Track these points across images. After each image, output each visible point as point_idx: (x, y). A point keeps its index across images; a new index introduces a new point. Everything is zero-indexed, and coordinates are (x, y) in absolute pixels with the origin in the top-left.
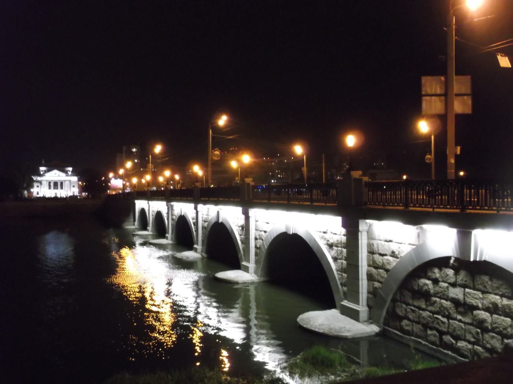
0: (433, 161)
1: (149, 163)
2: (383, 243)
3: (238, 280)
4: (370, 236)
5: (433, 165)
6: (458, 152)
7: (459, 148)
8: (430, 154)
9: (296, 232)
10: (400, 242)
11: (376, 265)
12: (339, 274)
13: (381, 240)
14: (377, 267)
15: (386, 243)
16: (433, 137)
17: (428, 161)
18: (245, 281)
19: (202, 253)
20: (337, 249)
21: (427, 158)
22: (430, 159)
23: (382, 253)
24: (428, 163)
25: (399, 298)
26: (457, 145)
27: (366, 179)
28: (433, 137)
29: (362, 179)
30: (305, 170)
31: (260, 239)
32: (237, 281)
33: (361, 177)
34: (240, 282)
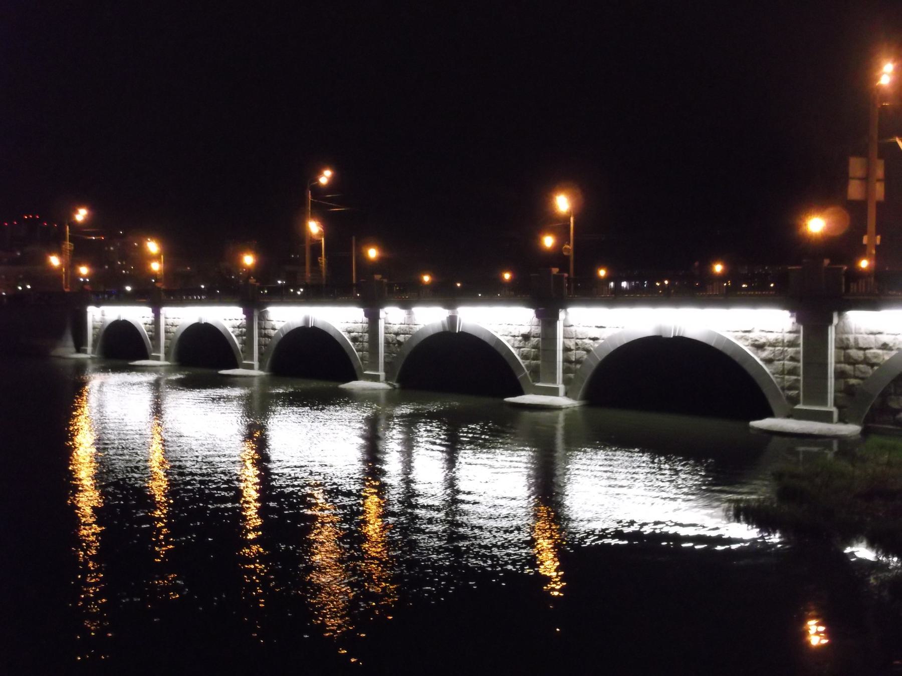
0: (571, 253)
1: (65, 239)
2: (866, 336)
3: (561, 405)
4: (840, 330)
5: (572, 258)
6: (878, 242)
7: (879, 237)
8: (569, 244)
9: (681, 335)
10: (896, 334)
11: (852, 361)
12: (776, 378)
13: (861, 333)
14: (853, 362)
15: (872, 337)
16: (572, 219)
17: (565, 253)
18: (568, 406)
19: (389, 382)
20: (775, 350)
21: (566, 248)
22: (568, 250)
23: (864, 347)
24: (565, 256)
25: (892, 391)
26: (877, 234)
27: (385, 280)
28: (572, 219)
29: (383, 281)
30: (323, 261)
31: (578, 349)
32: (560, 406)
33: (382, 280)
34: (564, 407)
